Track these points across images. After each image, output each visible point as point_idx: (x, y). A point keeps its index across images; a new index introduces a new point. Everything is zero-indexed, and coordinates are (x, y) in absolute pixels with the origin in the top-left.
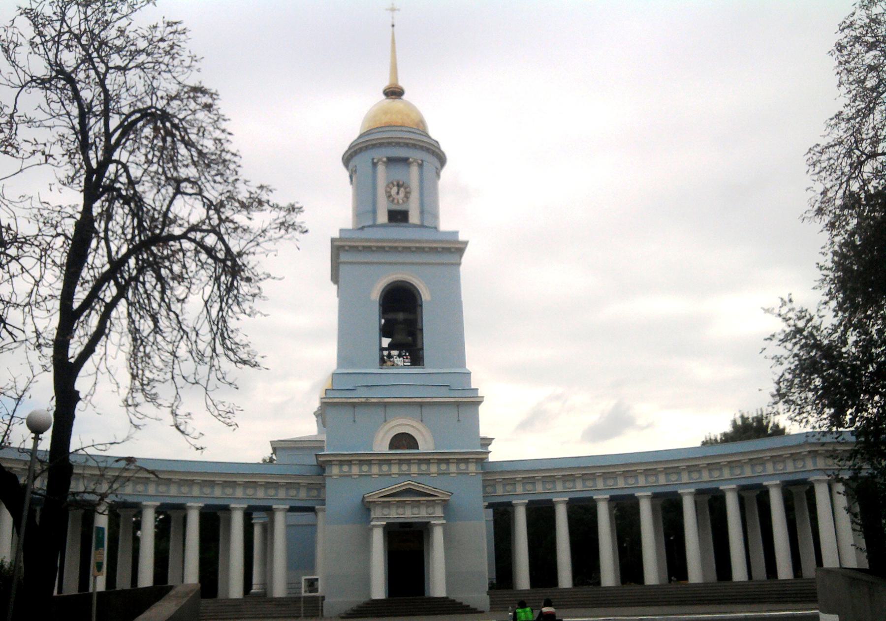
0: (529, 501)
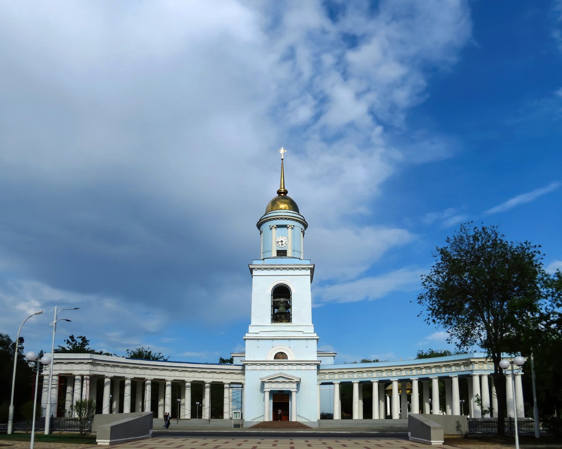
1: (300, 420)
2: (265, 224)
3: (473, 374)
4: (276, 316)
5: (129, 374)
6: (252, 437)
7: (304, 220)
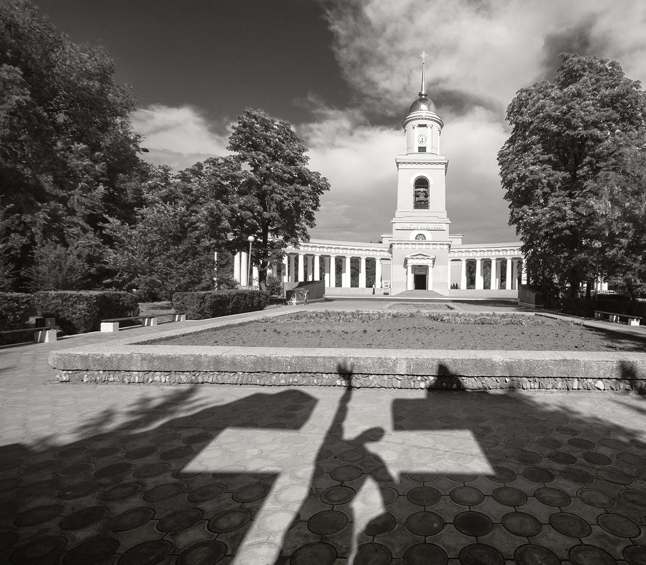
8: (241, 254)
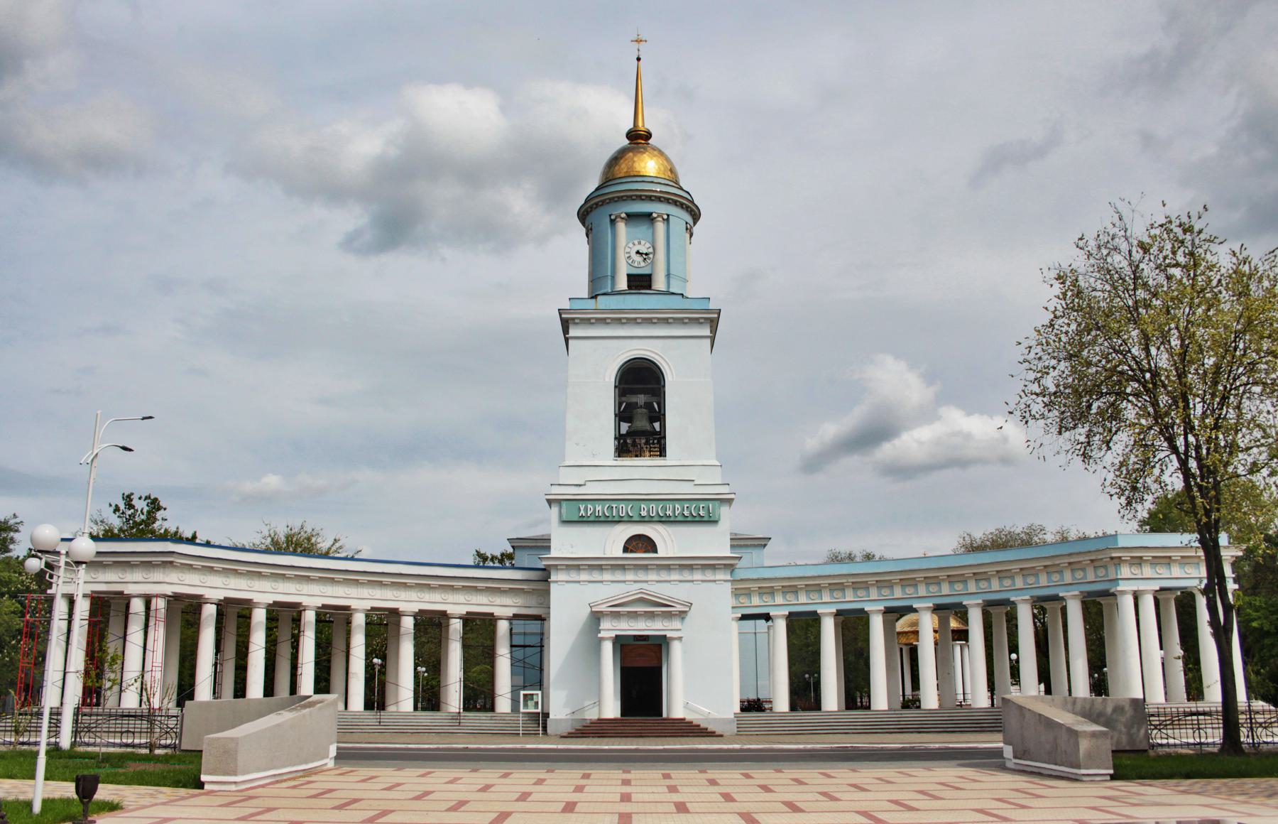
0: (790, 613)
1: (689, 717)
2: (597, 210)
3: (1119, 588)
4: (625, 442)
5: (263, 593)
6: (452, 763)
7: (692, 202)
8: (86, 620)
